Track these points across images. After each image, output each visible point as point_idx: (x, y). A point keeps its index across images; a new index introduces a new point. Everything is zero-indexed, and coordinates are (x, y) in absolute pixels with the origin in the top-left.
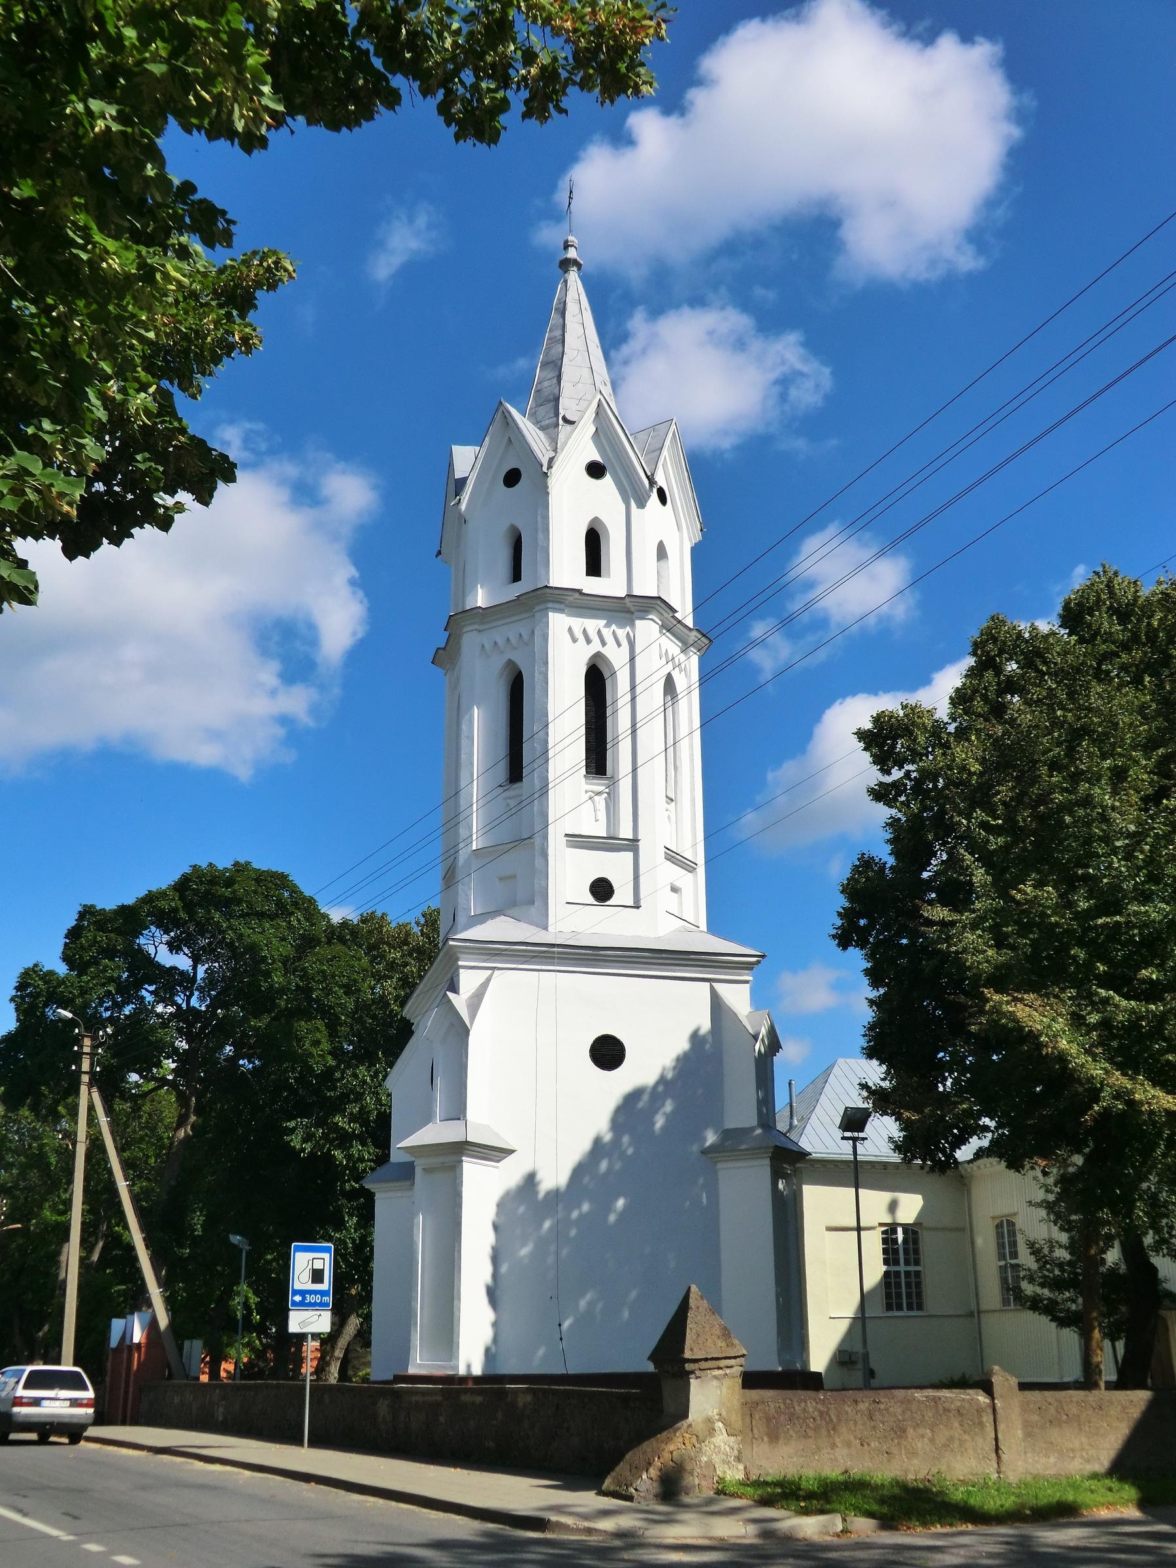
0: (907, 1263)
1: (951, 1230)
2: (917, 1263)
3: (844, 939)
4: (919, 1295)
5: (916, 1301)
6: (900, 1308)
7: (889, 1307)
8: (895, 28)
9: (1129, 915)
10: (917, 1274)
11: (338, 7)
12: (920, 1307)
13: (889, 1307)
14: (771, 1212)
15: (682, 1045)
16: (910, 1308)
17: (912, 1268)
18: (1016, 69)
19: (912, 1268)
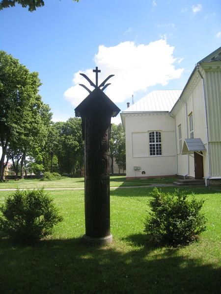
0: (157, 142)
1: (169, 132)
2: (160, 141)
3: (167, 44)
4: (160, 151)
5: (159, 152)
6: (154, 154)
7: (151, 154)
8: (13, 198)
9: (198, 68)
10: (160, 145)
11: (103, 160)
12: (161, 154)
13: (151, 154)
14: (112, 100)
15: (152, 44)
16: (157, 154)
17: (159, 143)
18: (101, 44)
19: (159, 143)
